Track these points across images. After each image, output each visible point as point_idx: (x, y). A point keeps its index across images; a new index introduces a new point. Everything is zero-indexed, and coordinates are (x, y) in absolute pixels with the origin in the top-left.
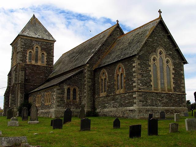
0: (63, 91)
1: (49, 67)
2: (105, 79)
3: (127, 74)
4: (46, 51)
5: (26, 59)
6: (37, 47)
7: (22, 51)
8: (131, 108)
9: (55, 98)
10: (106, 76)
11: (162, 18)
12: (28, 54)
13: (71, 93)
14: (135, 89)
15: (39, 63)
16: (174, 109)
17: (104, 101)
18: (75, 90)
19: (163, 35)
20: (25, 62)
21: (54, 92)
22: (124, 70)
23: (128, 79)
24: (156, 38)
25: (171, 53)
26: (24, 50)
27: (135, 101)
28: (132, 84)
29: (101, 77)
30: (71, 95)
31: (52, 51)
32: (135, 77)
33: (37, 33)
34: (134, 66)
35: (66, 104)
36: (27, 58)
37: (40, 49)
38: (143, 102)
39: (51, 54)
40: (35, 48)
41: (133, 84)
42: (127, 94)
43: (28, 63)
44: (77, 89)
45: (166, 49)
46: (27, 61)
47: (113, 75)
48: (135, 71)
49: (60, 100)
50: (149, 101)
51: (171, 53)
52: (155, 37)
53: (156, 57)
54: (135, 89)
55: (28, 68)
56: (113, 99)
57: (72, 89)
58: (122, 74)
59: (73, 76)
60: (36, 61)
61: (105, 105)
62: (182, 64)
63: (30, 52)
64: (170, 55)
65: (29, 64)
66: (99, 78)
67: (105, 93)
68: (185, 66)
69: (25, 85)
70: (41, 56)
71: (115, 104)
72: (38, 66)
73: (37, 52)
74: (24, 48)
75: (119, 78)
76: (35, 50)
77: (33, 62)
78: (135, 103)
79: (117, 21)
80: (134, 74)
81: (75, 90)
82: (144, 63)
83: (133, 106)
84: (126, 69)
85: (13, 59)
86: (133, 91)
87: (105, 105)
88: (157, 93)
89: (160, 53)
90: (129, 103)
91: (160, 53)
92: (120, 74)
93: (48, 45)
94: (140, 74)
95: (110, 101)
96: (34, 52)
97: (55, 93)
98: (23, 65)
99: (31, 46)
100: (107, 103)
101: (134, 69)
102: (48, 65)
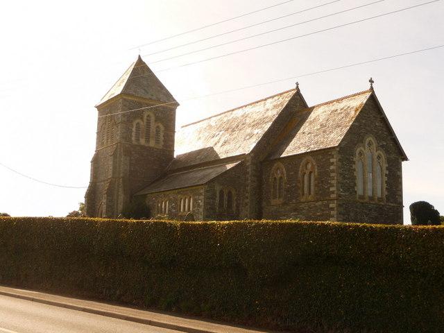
2: (281, 178)
5: (131, 136)
6: (148, 116)
9: (201, 204)
10: (282, 173)
11: (373, 92)
14: (333, 196)
15: (152, 144)
16: (227, 225)
17: (279, 212)
19: (374, 117)
20: (130, 140)
21: (201, 194)
22: (316, 167)
23: (322, 182)
24: (364, 121)
25: (385, 143)
28: (329, 188)
29: (273, 174)
34: (333, 163)
36: (133, 134)
37: (153, 118)
38: (344, 215)
40: (145, 117)
42: (320, 203)
43: (134, 143)
44: (233, 192)
45: (378, 138)
46: (133, 139)
47: (296, 173)
48: (333, 169)
50: (352, 214)
51: (385, 143)
52: (363, 119)
53: (363, 149)
54: (333, 196)
56: (295, 210)
58: (311, 173)
60: (148, 140)
63: (138, 123)
64: (382, 146)
67: (281, 200)
68: (404, 164)
72: (150, 148)
75: (306, 178)
77: (143, 141)
78: (333, 217)
79: (297, 84)
80: (332, 175)
82: (347, 159)
83: (440, 224)
84: (318, 166)
88: (362, 203)
89: (370, 144)
90: (322, 216)
91: (370, 144)
92: (307, 172)
94: (341, 174)
96: (143, 124)
97: (202, 197)
98: (127, 146)
101: (332, 167)
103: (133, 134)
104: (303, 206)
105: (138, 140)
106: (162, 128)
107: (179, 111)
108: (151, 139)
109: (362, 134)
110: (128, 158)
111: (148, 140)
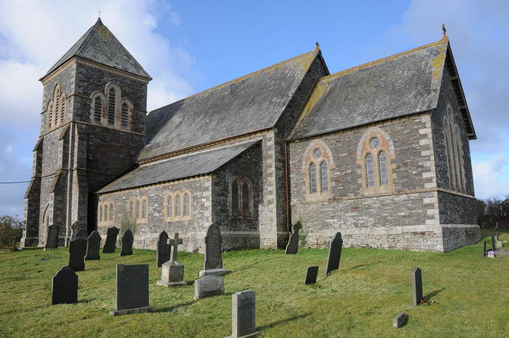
0: (226, 189)
1: (136, 135)
3: (401, 154)
4: (131, 99)
5: (90, 114)
7: (79, 93)
8: (420, 228)
10: (326, 155)
12: (94, 102)
13: (240, 192)
15: (117, 125)
18: (245, 186)
21: (207, 189)
26: (85, 93)
27: (430, 212)
30: (239, 198)
31: (143, 100)
32: (429, 160)
33: (112, 58)
35: (232, 220)
36: (92, 111)
37: (118, 93)
39: (142, 106)
41: (423, 174)
42: (404, 197)
43: (93, 122)
46: (92, 117)
47: (352, 153)
49: (221, 210)
55: (93, 134)
56: (355, 208)
57: (242, 183)
59: (166, 162)
60: (111, 121)
61: (327, 221)
62: (468, 139)
65: (96, 126)
66: (300, 161)
69: (87, 172)
70: (121, 110)
71: (362, 220)
72: (115, 131)
73: (112, 98)
74: (86, 88)
76: (108, 95)
77: (104, 122)
78: (432, 217)
80: (424, 153)
81: (245, 186)
85: (48, 113)
86: (422, 190)
87: (327, 221)
90: (410, 216)
93: (135, 85)
95: (343, 213)
99: (100, 86)
100: (333, 217)
102: (136, 130)
103: (92, 111)
104: (369, 202)
105: (98, 119)
106: (130, 106)
107: (150, 86)
108: (115, 121)
109: (14, 260)
110: (85, 143)
111: (111, 121)
